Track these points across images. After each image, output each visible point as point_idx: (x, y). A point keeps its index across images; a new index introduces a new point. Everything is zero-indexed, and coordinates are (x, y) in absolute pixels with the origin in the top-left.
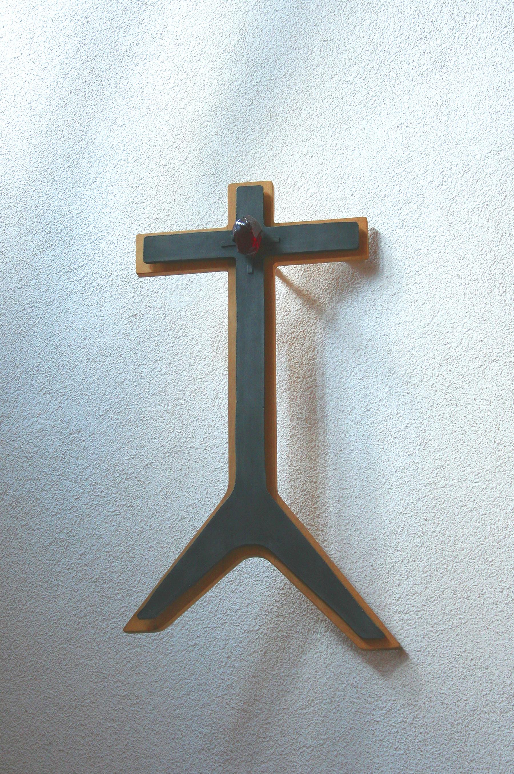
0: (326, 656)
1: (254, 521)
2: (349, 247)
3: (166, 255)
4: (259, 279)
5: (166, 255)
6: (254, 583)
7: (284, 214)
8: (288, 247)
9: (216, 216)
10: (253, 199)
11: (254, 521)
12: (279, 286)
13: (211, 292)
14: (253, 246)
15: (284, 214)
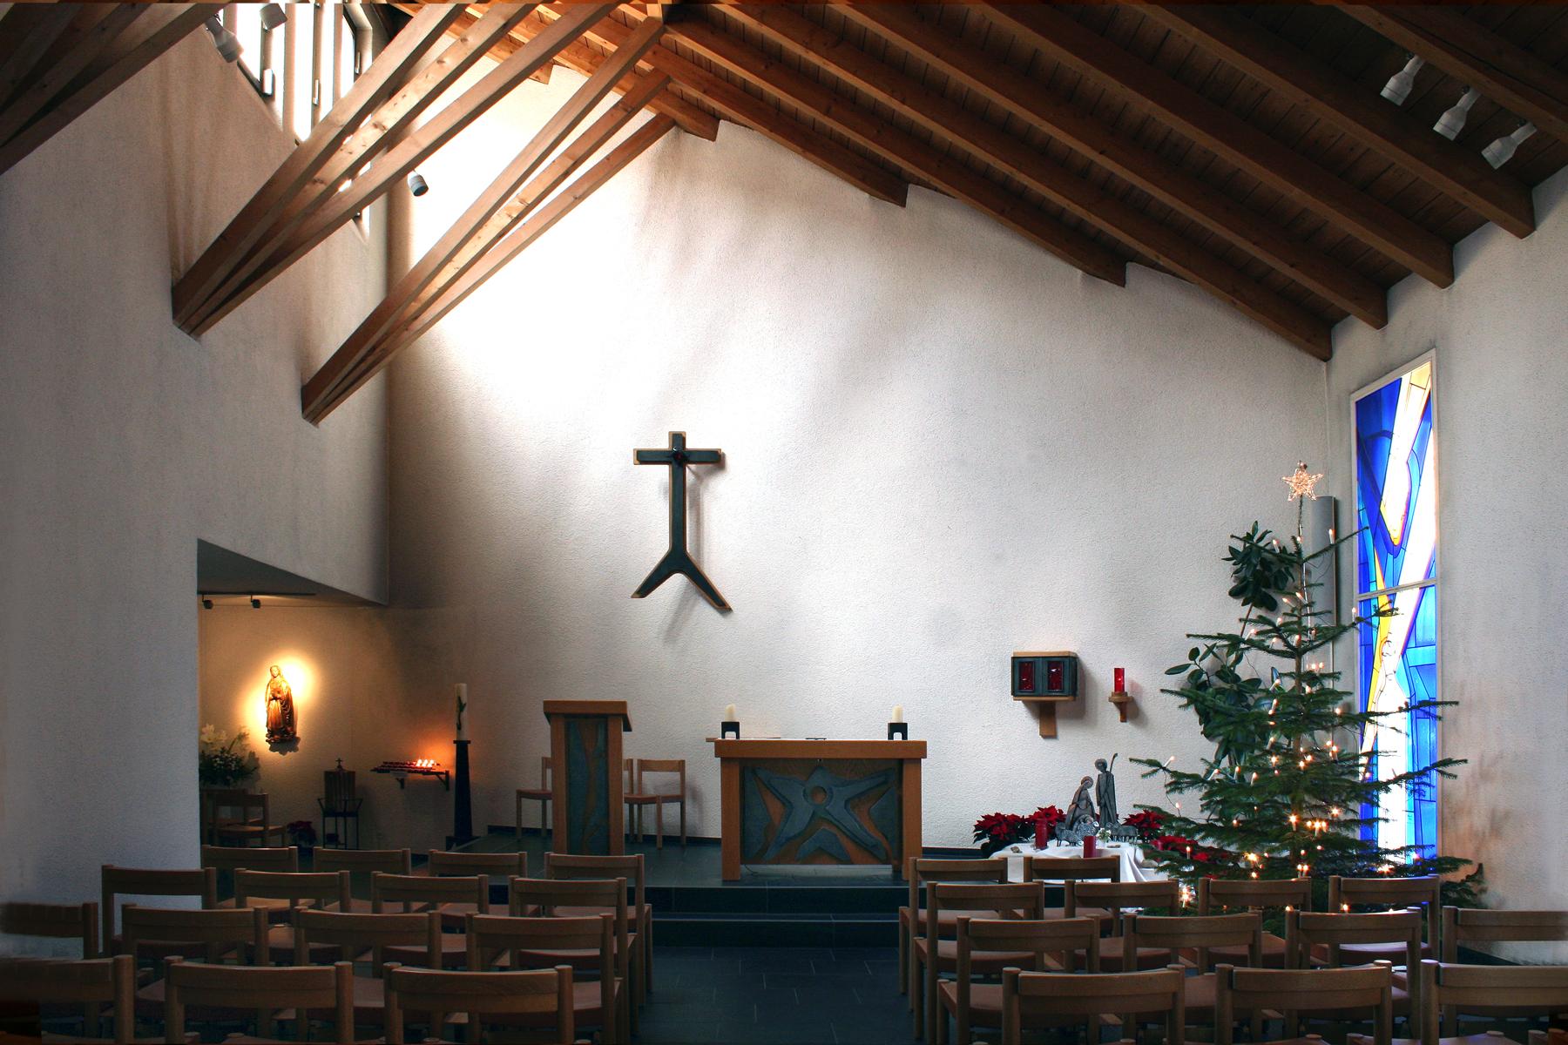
0: (704, 609)
1: (679, 560)
2: (714, 460)
3: (644, 457)
6: (677, 581)
7: (690, 445)
9: (664, 444)
10: (678, 438)
11: (679, 560)
13: (663, 472)
14: (678, 456)
15: (690, 445)
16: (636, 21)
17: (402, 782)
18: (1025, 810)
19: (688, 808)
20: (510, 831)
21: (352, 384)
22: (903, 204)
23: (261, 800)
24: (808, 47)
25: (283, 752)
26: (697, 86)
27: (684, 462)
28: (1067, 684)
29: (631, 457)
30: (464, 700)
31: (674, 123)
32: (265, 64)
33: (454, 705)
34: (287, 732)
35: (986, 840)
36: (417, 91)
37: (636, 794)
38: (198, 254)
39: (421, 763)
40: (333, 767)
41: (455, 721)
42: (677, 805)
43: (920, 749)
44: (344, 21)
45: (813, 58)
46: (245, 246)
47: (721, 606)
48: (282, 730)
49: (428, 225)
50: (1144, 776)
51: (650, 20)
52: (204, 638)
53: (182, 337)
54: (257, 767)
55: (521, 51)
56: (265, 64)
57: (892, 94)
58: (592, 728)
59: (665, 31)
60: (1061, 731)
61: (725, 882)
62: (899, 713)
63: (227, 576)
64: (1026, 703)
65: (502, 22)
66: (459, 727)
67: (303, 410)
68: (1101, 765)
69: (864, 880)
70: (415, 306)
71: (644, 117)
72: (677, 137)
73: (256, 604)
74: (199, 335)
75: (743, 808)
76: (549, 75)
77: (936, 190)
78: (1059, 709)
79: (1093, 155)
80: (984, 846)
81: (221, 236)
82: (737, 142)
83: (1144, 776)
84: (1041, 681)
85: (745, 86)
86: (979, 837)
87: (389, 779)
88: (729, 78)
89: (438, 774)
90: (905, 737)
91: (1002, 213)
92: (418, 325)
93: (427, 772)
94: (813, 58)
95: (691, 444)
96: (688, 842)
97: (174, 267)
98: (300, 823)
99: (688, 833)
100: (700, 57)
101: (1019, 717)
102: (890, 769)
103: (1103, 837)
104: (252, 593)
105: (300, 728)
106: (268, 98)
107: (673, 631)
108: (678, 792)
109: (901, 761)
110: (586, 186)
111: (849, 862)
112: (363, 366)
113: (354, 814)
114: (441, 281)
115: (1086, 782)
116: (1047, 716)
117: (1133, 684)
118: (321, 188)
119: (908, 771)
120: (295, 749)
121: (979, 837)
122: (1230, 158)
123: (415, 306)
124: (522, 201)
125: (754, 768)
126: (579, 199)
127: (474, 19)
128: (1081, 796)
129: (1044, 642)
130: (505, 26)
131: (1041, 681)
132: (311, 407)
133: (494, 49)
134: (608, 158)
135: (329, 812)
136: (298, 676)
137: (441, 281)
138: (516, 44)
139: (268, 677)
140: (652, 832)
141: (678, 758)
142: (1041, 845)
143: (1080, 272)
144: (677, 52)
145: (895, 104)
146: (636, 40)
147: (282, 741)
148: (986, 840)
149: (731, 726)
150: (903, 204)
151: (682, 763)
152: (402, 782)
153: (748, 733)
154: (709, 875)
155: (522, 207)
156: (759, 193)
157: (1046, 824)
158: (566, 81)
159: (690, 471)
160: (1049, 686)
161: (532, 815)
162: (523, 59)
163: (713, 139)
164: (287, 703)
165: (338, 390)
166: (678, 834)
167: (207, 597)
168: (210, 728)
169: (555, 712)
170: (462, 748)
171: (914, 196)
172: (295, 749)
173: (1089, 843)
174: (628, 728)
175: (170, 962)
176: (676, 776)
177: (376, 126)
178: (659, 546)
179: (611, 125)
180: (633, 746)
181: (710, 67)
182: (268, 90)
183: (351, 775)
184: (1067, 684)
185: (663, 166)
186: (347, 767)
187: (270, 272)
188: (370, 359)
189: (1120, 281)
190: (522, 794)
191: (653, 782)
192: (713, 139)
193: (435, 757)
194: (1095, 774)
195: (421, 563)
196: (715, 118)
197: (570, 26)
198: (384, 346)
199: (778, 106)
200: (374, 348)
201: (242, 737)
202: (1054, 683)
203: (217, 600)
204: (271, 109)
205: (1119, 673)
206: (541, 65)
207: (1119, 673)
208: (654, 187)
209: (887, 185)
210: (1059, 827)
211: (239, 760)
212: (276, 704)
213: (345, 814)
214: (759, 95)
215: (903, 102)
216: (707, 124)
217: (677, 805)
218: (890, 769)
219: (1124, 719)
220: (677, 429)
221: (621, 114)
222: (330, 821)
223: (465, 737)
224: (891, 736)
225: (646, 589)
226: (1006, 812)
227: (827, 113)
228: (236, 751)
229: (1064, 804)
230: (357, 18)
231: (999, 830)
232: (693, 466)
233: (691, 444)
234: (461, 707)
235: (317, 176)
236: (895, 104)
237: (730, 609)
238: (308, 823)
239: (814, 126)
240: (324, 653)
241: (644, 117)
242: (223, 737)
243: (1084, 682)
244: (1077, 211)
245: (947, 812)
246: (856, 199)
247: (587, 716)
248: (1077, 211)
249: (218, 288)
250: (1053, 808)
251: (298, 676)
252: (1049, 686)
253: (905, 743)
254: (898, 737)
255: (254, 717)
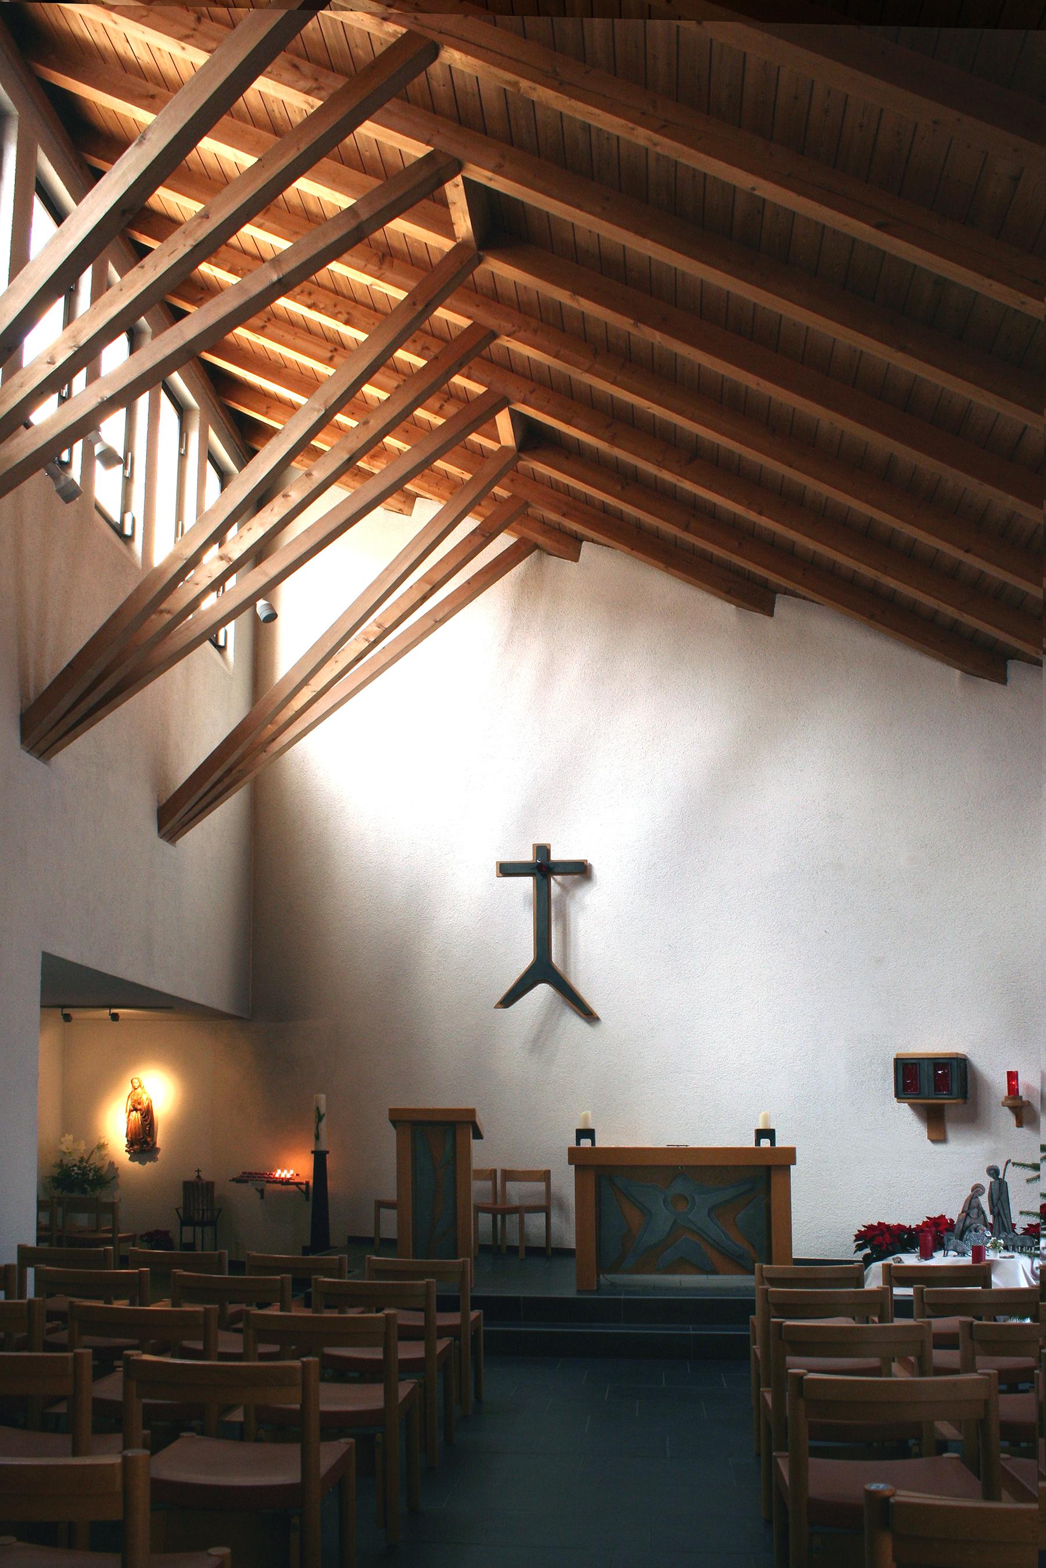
0: (573, 1021)
1: (543, 970)
2: (581, 871)
3: (507, 870)
4: (545, 881)
5: (507, 870)
6: (542, 992)
7: (554, 857)
8: (556, 870)
9: (528, 856)
10: (543, 851)
11: (543, 970)
12: (552, 881)
13: (527, 883)
14: (542, 868)
15: (554, 857)
16: (492, 451)
17: (262, 1192)
18: (912, 1219)
19: (554, 1220)
20: (371, 1241)
21: (207, 806)
22: (771, 614)
23: (111, 1208)
24: (661, 465)
25: (142, 1162)
26: (555, 509)
27: (549, 874)
28: (955, 1087)
29: (494, 869)
30: (323, 1110)
31: (536, 547)
32: (126, 508)
33: (313, 1116)
34: (147, 1143)
35: (868, 1251)
36: (262, 525)
37: (499, 1204)
38: (48, 681)
39: (280, 1174)
40: (191, 1176)
41: (314, 1131)
42: (541, 1217)
43: (790, 1155)
44: (208, 463)
45: (667, 476)
46: (93, 673)
47: (588, 1015)
48: (142, 1140)
49: (289, 652)
50: (1028, 1181)
51: (504, 449)
52: (66, 1054)
53: (30, 760)
54: (115, 1177)
55: (371, 481)
56: (126, 508)
57: (749, 506)
58: (440, 1137)
59: (520, 459)
60: (950, 1135)
61: (579, 1292)
62: (766, 1119)
63: (75, 991)
64: (911, 1105)
65: (346, 457)
66: (317, 1137)
67: (160, 829)
68: (993, 1172)
69: (718, 1290)
70: (271, 728)
71: (503, 542)
72: (540, 559)
73: (115, 1017)
74: (49, 759)
75: (599, 1218)
76: (412, 507)
77: (804, 598)
78: (949, 1113)
79: (958, 554)
80: (866, 1256)
81: (68, 665)
82: (600, 562)
83: (1028, 1181)
84: (926, 1082)
85: (604, 508)
86: (860, 1248)
87: (248, 1190)
88: (588, 500)
89: (297, 1184)
90: (773, 1143)
91: (872, 617)
92: (276, 746)
93: (286, 1182)
94: (667, 476)
95: (556, 856)
96: (550, 1253)
97: (24, 696)
98: (157, 1232)
99: (554, 1244)
100: (557, 482)
101: (906, 1120)
102: (758, 1176)
103: (995, 1246)
104: (111, 1007)
105: (161, 1138)
106: (128, 539)
107: (540, 1041)
108: (543, 1203)
109: (769, 1168)
110: (446, 610)
111: (714, 1272)
112: (220, 787)
113: (212, 1223)
114: (297, 703)
115: (977, 1190)
116: (936, 1123)
117: (1028, 1088)
118: (168, 617)
119: (776, 1179)
120: (155, 1159)
121: (860, 1248)
122: (960, 390)
123: (271, 728)
124: (379, 626)
125: (609, 1174)
126: (439, 622)
127: (322, 452)
128: (971, 1205)
129: (931, 1042)
130: (349, 459)
131: (926, 1082)
132: (169, 826)
133: (344, 478)
134: (468, 582)
135: (183, 1223)
136: (159, 1087)
137: (297, 703)
138: (318, 453)
139: (130, 1089)
140: (517, 1243)
141: (544, 1168)
142: (926, 1255)
143: (958, 672)
144: (535, 478)
145: (752, 516)
146: (490, 468)
147: (142, 1151)
148: (868, 1251)
149: (586, 1133)
150: (771, 614)
151: (547, 1173)
152: (262, 1192)
153: (603, 1141)
154: (565, 1286)
155: (378, 631)
156: (621, 610)
157: (935, 1233)
158: (428, 509)
159: (555, 884)
160: (936, 1089)
161: (390, 1225)
162: (373, 489)
163: (576, 560)
164: (147, 1114)
165: (196, 810)
166: (543, 1244)
167: (66, 1011)
168: (70, 1137)
169: (400, 1119)
170: (320, 1159)
171: (782, 606)
172: (155, 1159)
173: (978, 1253)
174: (478, 1135)
175: (130, 1356)
176: (541, 1186)
177: (221, 558)
178: (525, 957)
179: (469, 550)
180: (483, 1155)
181: (568, 490)
182: (128, 531)
183: (210, 1185)
184: (955, 1087)
185: (526, 589)
186: (206, 1177)
187: (119, 698)
188: (227, 781)
189: (1001, 678)
190: (381, 1204)
191: (517, 1191)
192: (576, 560)
193: (294, 1168)
194: (986, 1181)
195: (282, 975)
196: (577, 540)
197: (418, 458)
198: (240, 767)
199: (638, 525)
200: (230, 770)
201: (102, 1147)
202: (941, 1085)
203: (77, 1014)
204: (130, 550)
205: (1012, 1076)
206: (397, 492)
207: (1012, 1076)
208: (516, 610)
209: (754, 596)
210: (946, 1236)
211: (97, 1170)
212: (136, 1116)
213: (202, 1224)
214: (620, 516)
215: (760, 513)
216: (569, 546)
217: (541, 1217)
218: (758, 1176)
219: (1020, 1124)
220: (542, 841)
221: (479, 540)
222: (188, 1230)
223: (323, 1147)
224: (758, 1143)
225: (510, 999)
226: (891, 1221)
227: (686, 528)
228: (95, 1161)
229: (953, 1212)
230: (223, 463)
231: (880, 1239)
232: (558, 878)
233: (556, 856)
234: (320, 1118)
235: (163, 606)
236: (752, 516)
237: (598, 1019)
238: (166, 1233)
239: (675, 542)
240: (185, 1065)
241: (503, 542)
242: (82, 1147)
243: (975, 1087)
244: (950, 611)
245: (821, 1222)
246: (722, 611)
247: (430, 1123)
248: (950, 611)
249: (63, 717)
250: (942, 1217)
251: (159, 1087)
252: (936, 1089)
253: (773, 1151)
254: (765, 1143)
255: (114, 1127)
